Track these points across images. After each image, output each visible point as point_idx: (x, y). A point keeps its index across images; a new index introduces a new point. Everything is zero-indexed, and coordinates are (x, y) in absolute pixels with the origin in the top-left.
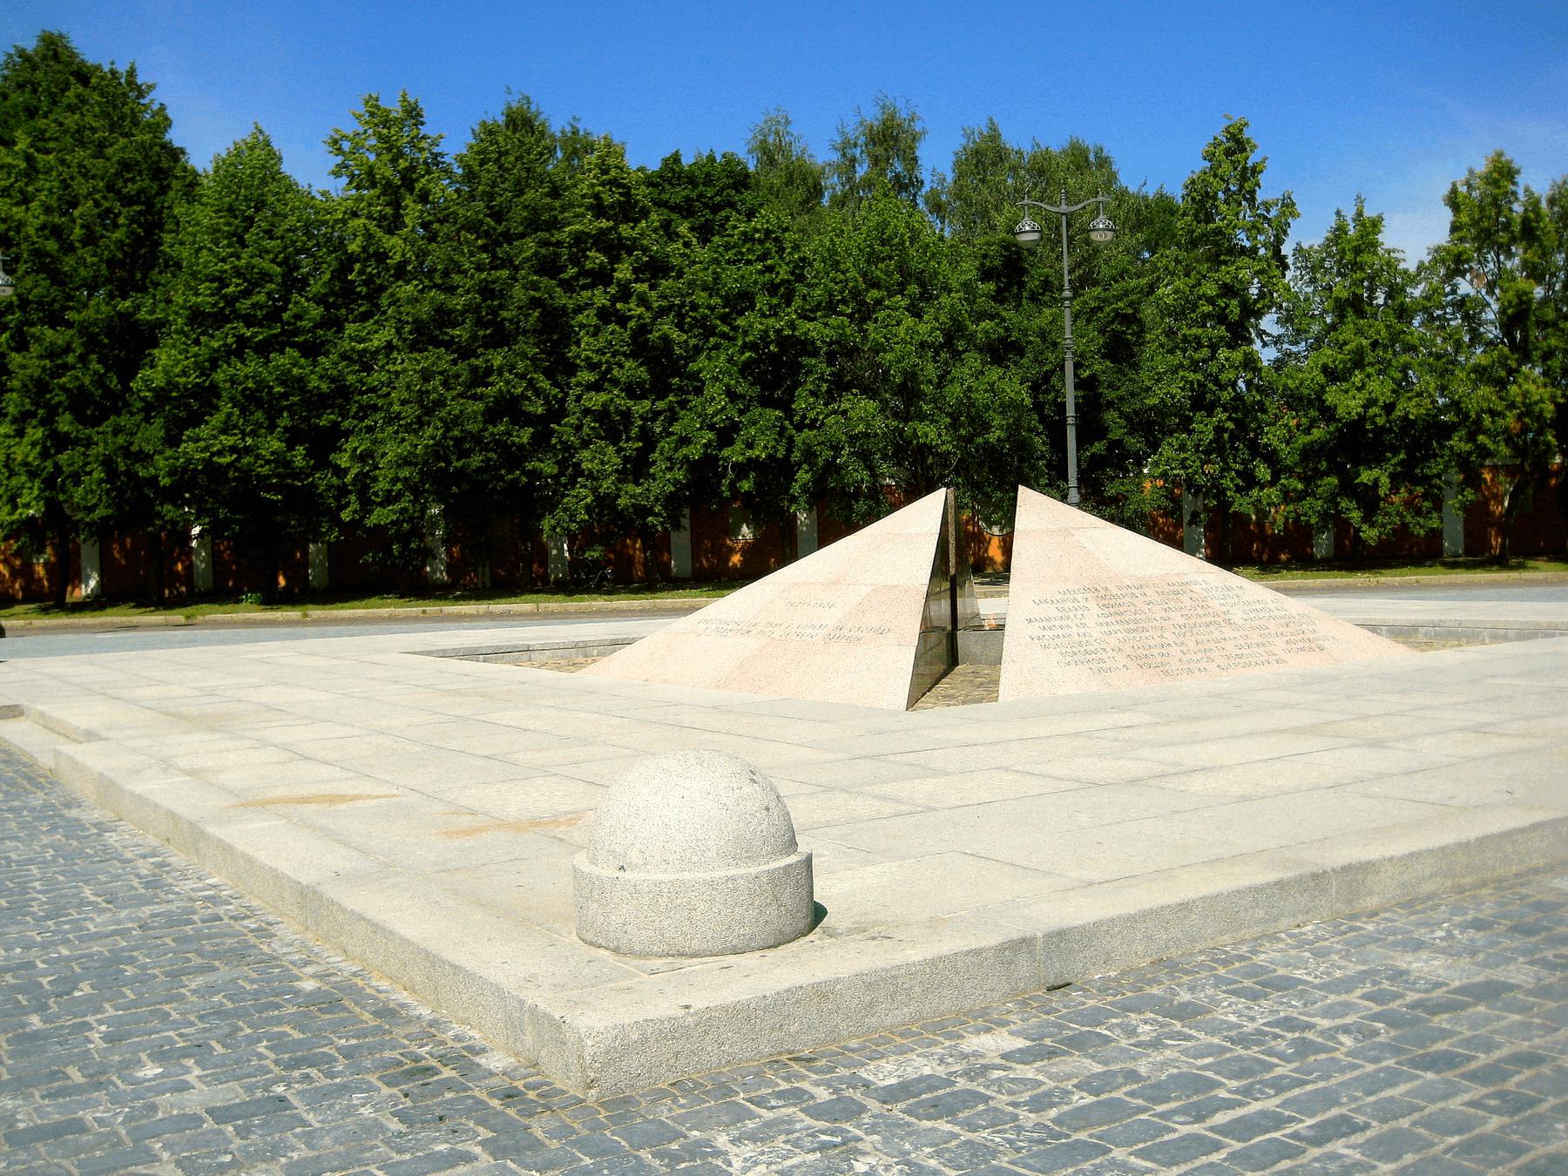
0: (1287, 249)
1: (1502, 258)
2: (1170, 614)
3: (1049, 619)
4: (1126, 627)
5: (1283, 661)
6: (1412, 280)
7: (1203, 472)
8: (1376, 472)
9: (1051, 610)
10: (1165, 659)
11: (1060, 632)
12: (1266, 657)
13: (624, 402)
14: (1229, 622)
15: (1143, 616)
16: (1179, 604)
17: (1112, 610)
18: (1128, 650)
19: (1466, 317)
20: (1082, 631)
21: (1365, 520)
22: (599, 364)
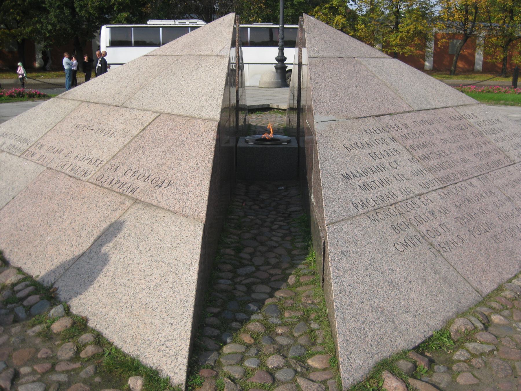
3: (366, 173)
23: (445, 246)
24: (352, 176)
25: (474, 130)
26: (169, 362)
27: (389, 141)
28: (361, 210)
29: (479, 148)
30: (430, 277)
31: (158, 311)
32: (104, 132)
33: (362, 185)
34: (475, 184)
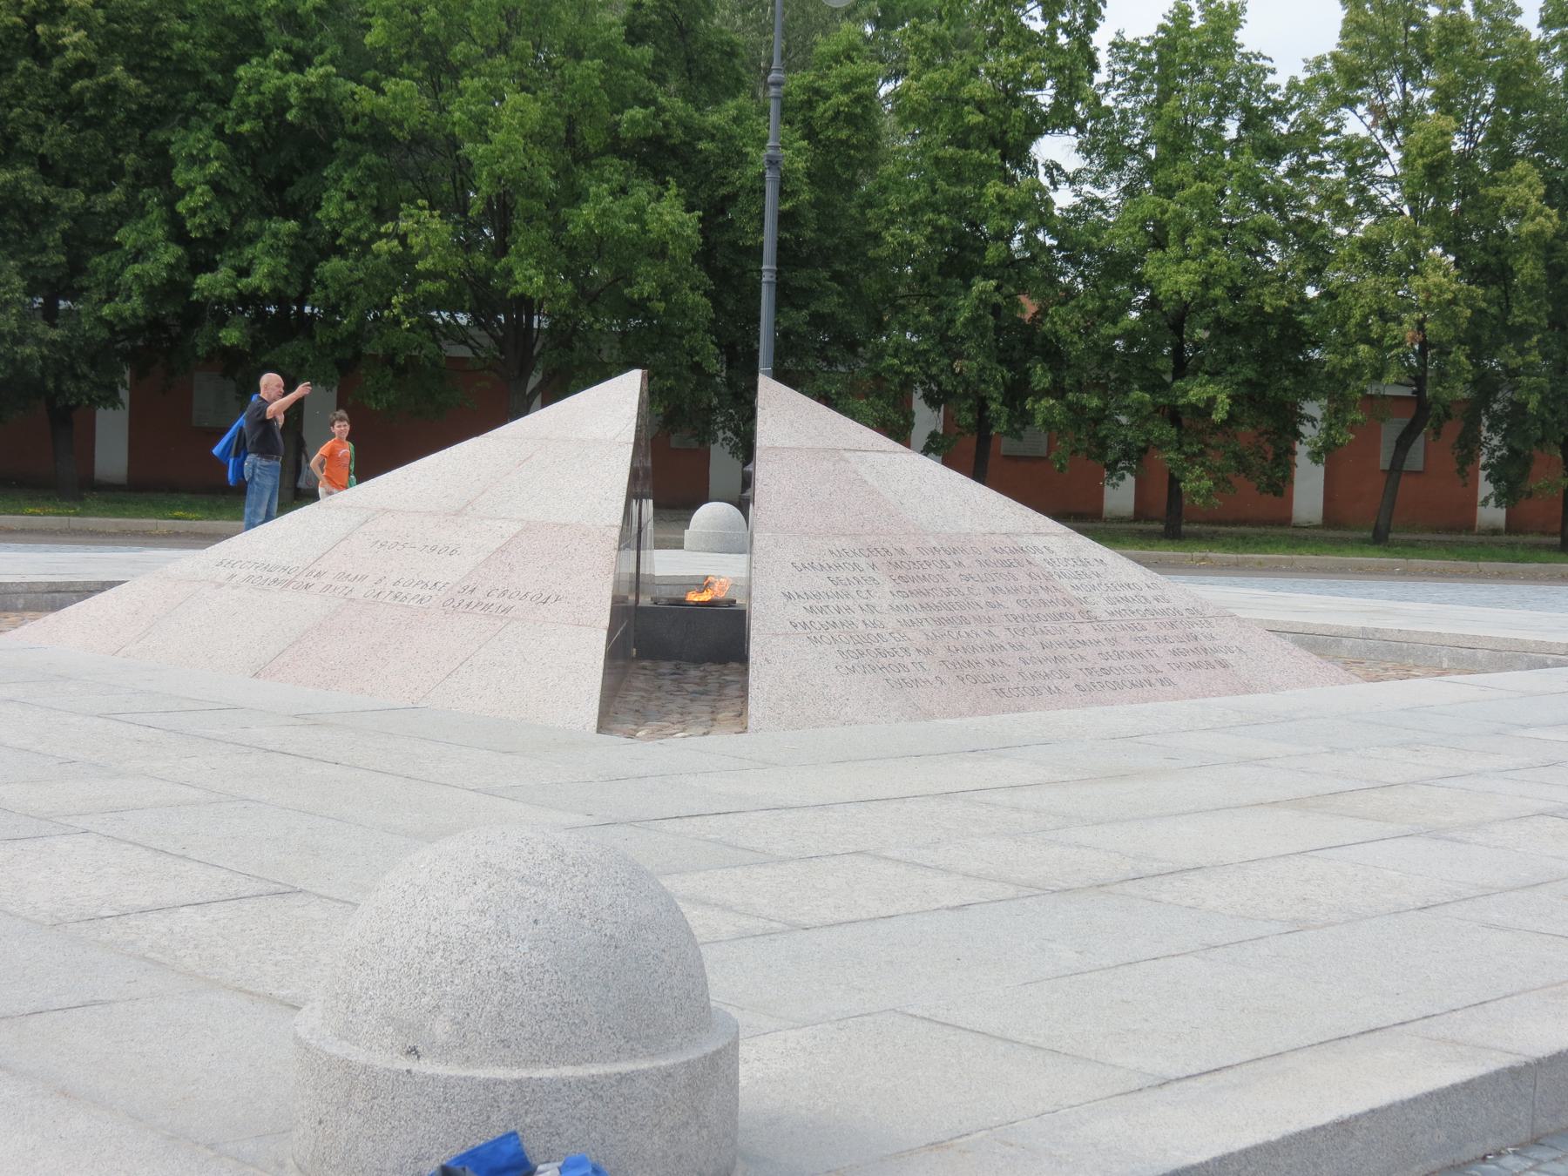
0: (1101, 40)
1: (1409, 87)
2: (1001, 598)
3: (817, 596)
4: (935, 614)
5: (1171, 683)
6: (1279, 110)
8: (1211, 389)
9: (819, 581)
10: (999, 670)
11: (837, 618)
12: (1145, 675)
13: (39, 191)
14: (1090, 618)
15: (960, 598)
16: (1012, 583)
17: (913, 586)
18: (941, 653)
19: (1352, 171)
20: (870, 617)
25: (1035, 570)
28: (800, 629)
29: (1033, 593)
32: (438, 549)
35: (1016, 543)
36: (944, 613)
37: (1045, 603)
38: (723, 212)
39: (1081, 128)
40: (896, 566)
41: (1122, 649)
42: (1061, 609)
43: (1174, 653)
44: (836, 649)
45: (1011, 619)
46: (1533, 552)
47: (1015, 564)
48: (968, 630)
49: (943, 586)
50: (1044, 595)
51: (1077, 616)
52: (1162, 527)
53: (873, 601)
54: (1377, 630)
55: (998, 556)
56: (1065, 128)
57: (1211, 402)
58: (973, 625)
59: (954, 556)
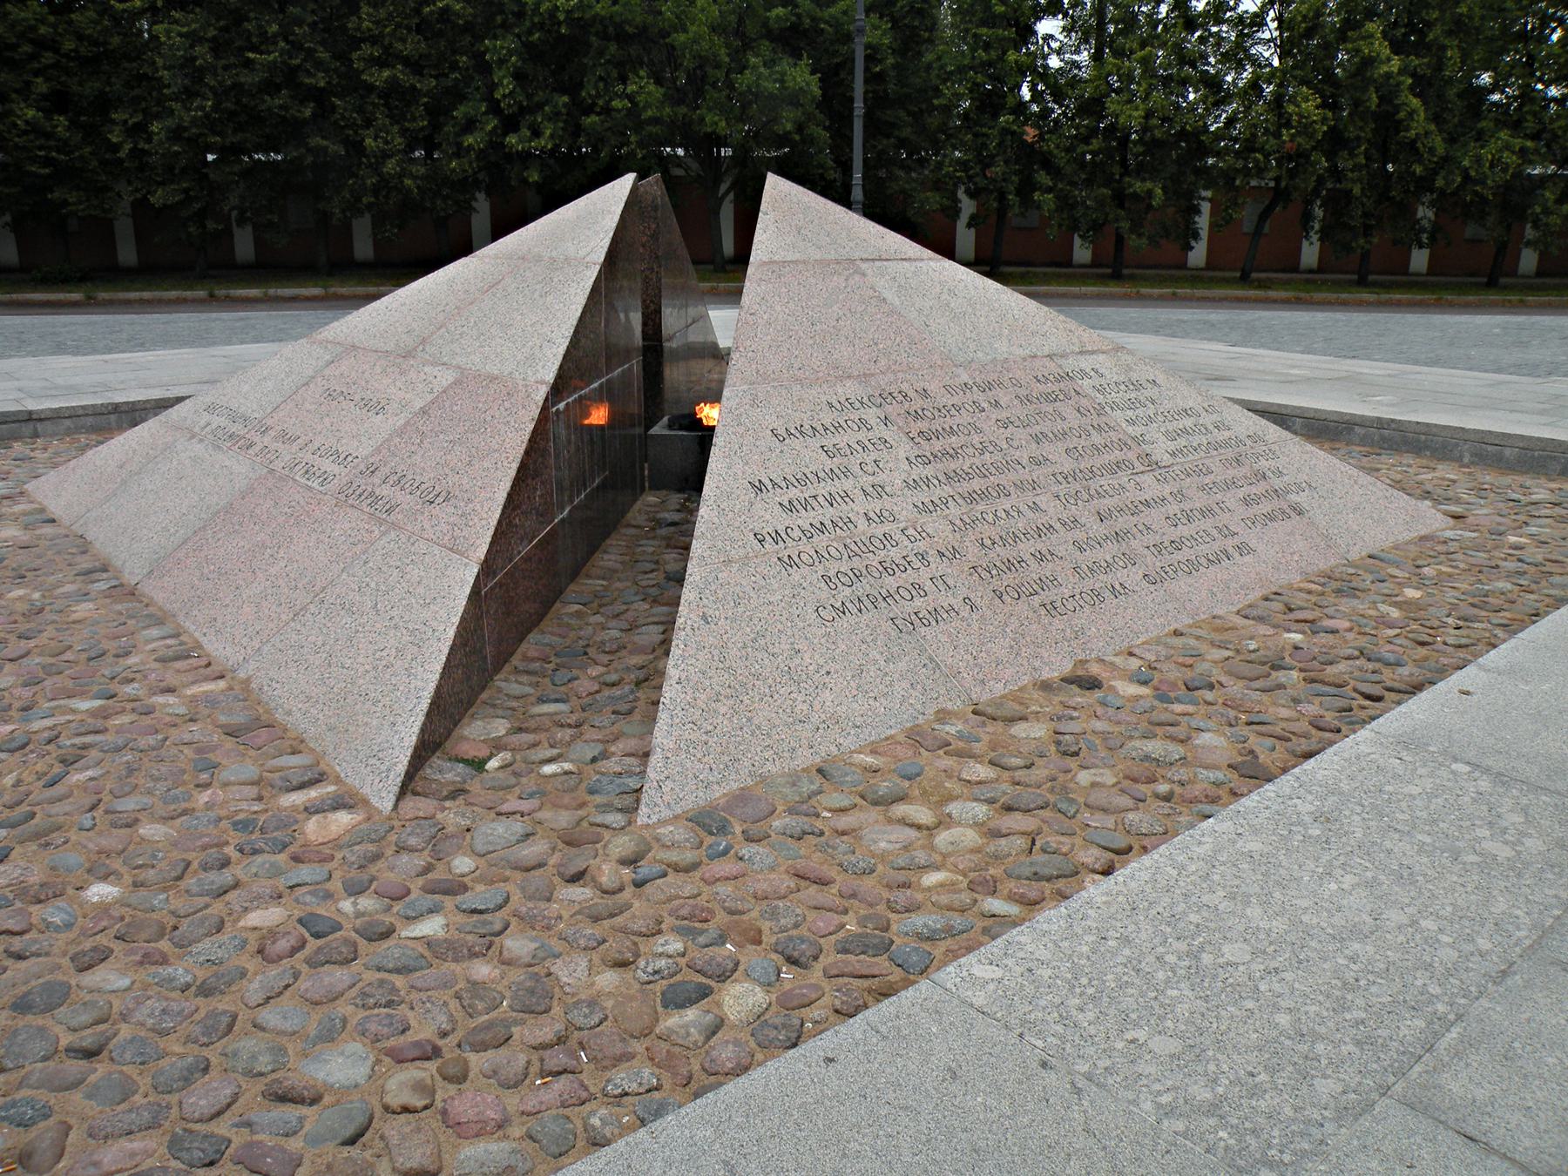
2: (1048, 449)
3: (802, 481)
5: (1251, 551)
7: (985, 175)
8: (1149, 185)
9: (809, 456)
10: (1048, 569)
14: (1153, 465)
16: (1060, 425)
17: (937, 445)
18: (973, 553)
20: (876, 505)
21: (1132, 231)
22: (382, 36)
23: (928, 616)
24: (770, 487)
25: (1084, 402)
26: (377, 780)
27: (874, 425)
29: (1084, 436)
30: (872, 668)
31: (381, 704)
33: (786, 503)
34: (1043, 507)
35: (1060, 366)
36: (977, 484)
37: (1098, 450)
38: (837, 74)
39: (1065, 15)
40: (917, 416)
41: (1190, 506)
42: (1117, 455)
43: (1246, 502)
44: (820, 573)
45: (1060, 478)
46: (1339, 286)
47: (1061, 397)
48: (1008, 507)
49: (976, 439)
50: (1097, 439)
51: (1137, 464)
52: (1109, 271)
53: (881, 478)
54: (1393, 421)
55: (1041, 387)
56: (1055, 15)
57: (1150, 193)
58: (1014, 496)
59: (990, 393)
